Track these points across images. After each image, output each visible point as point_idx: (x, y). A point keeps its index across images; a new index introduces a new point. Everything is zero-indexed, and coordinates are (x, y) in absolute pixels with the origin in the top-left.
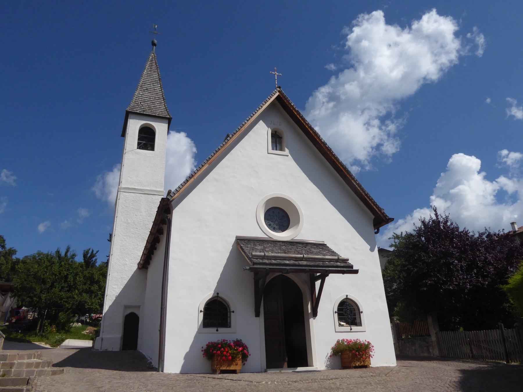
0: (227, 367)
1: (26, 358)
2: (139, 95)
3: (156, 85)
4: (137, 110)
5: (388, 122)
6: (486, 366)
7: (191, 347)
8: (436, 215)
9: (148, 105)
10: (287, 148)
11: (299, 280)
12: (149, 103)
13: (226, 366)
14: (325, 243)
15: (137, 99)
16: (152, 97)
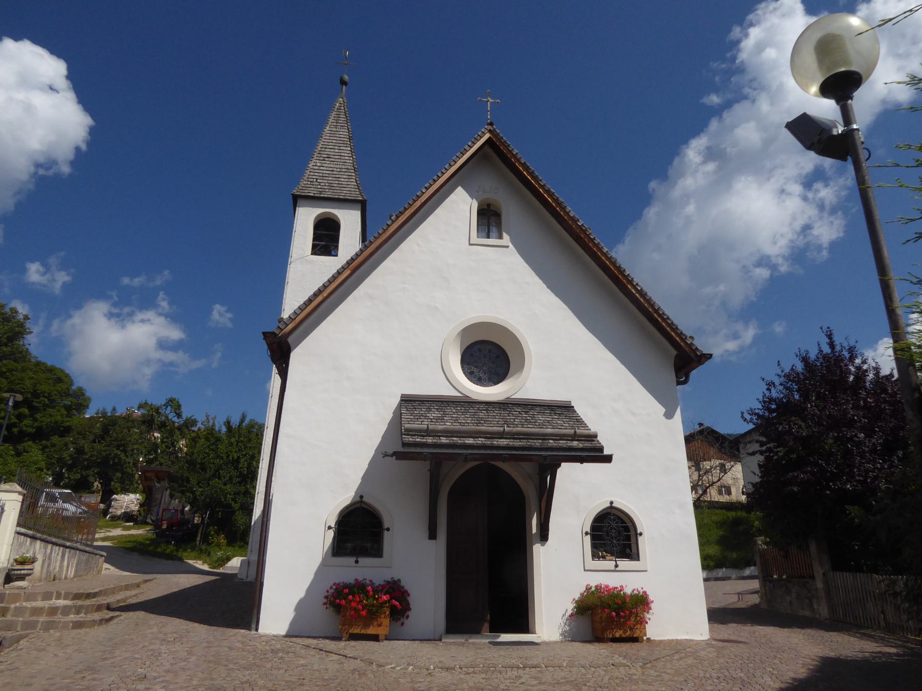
0: (362, 629)
1: (40, 599)
2: (315, 167)
3: (344, 148)
4: (310, 191)
5: (818, 185)
6: (893, 650)
7: (309, 590)
8: (832, 345)
9: (329, 182)
10: (506, 233)
11: (517, 472)
12: (331, 179)
13: (360, 627)
14: (572, 405)
15: (312, 174)
16: (335, 170)
